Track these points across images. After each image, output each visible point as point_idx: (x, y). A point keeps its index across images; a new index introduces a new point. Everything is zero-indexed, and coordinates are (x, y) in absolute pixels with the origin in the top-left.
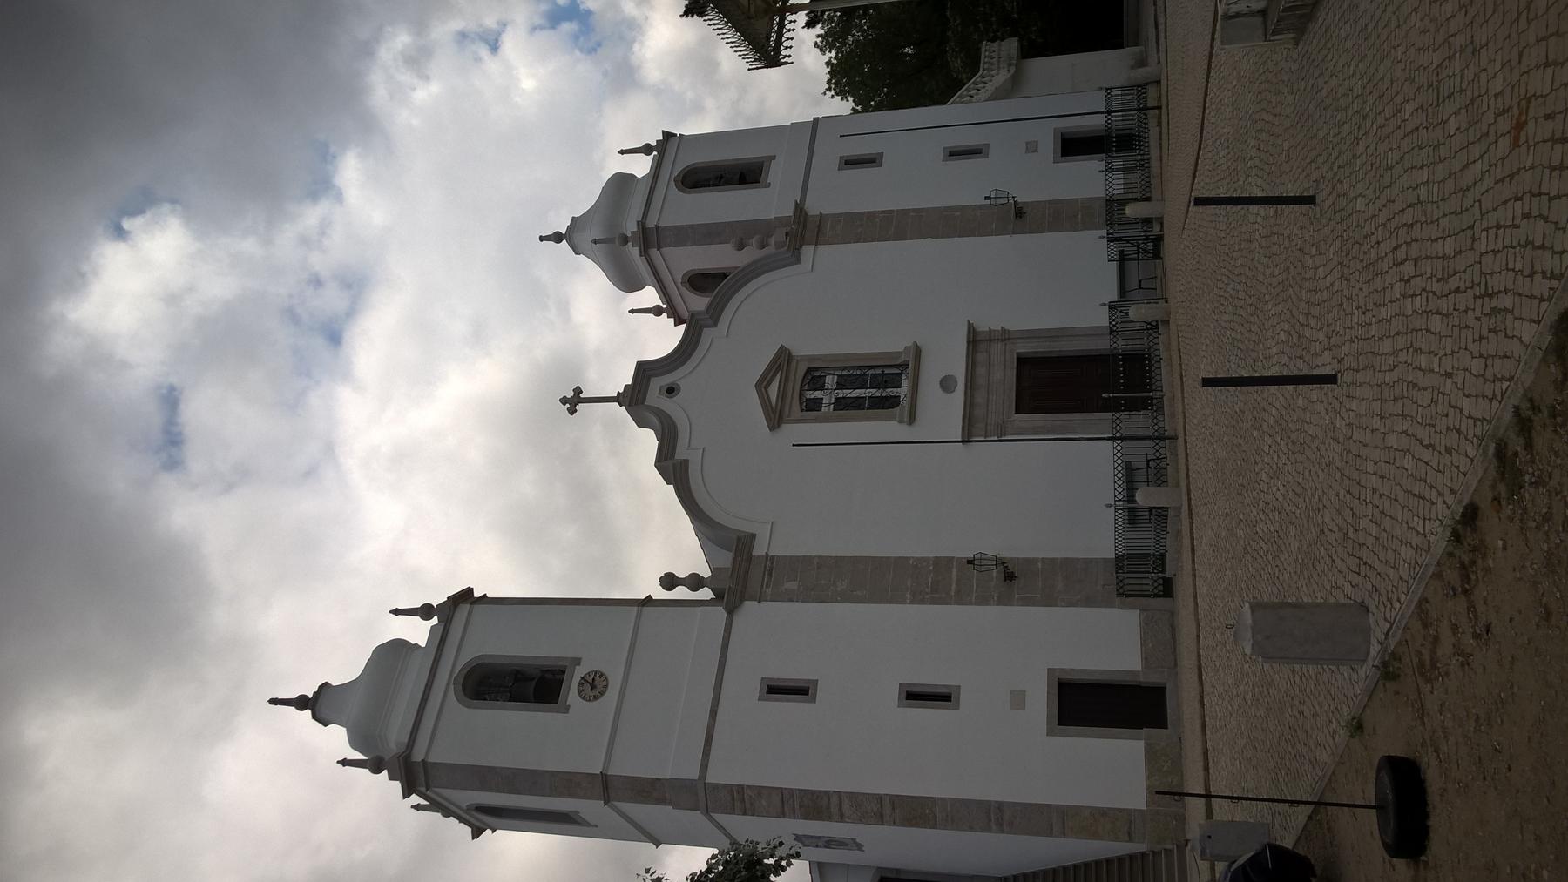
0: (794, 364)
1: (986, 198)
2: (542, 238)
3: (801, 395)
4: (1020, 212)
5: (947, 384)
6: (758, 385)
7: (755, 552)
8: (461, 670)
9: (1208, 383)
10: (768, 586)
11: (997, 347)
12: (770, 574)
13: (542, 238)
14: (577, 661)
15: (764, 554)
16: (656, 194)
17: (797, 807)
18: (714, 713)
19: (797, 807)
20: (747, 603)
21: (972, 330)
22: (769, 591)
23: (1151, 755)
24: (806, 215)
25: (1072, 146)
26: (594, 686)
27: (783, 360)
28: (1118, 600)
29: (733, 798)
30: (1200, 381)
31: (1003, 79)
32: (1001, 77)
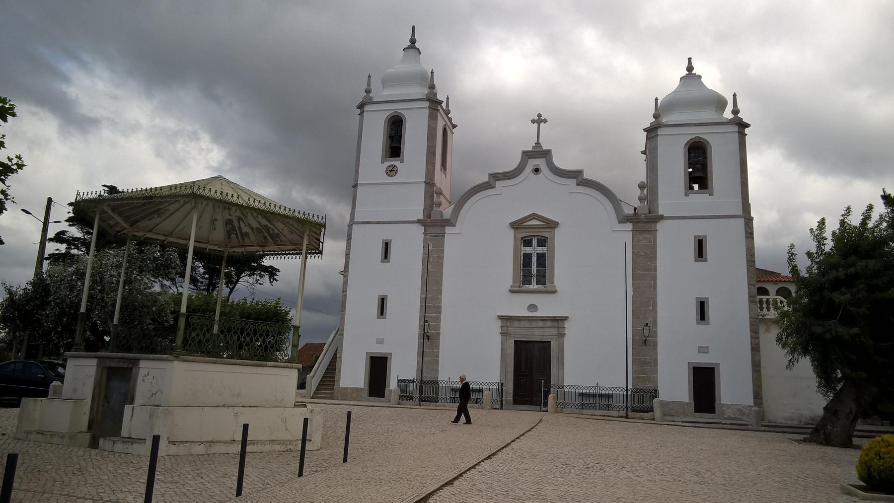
0: (549, 230)
2: (690, 59)
5: (532, 307)
6: (534, 214)
8: (400, 113)
9: (349, 413)
10: (430, 236)
12: (436, 236)
13: (690, 59)
16: (676, 129)
18: (378, 223)
21: (564, 319)
22: (429, 237)
23: (357, 390)
24: (657, 222)
26: (392, 171)
27: (552, 225)
30: (350, 411)
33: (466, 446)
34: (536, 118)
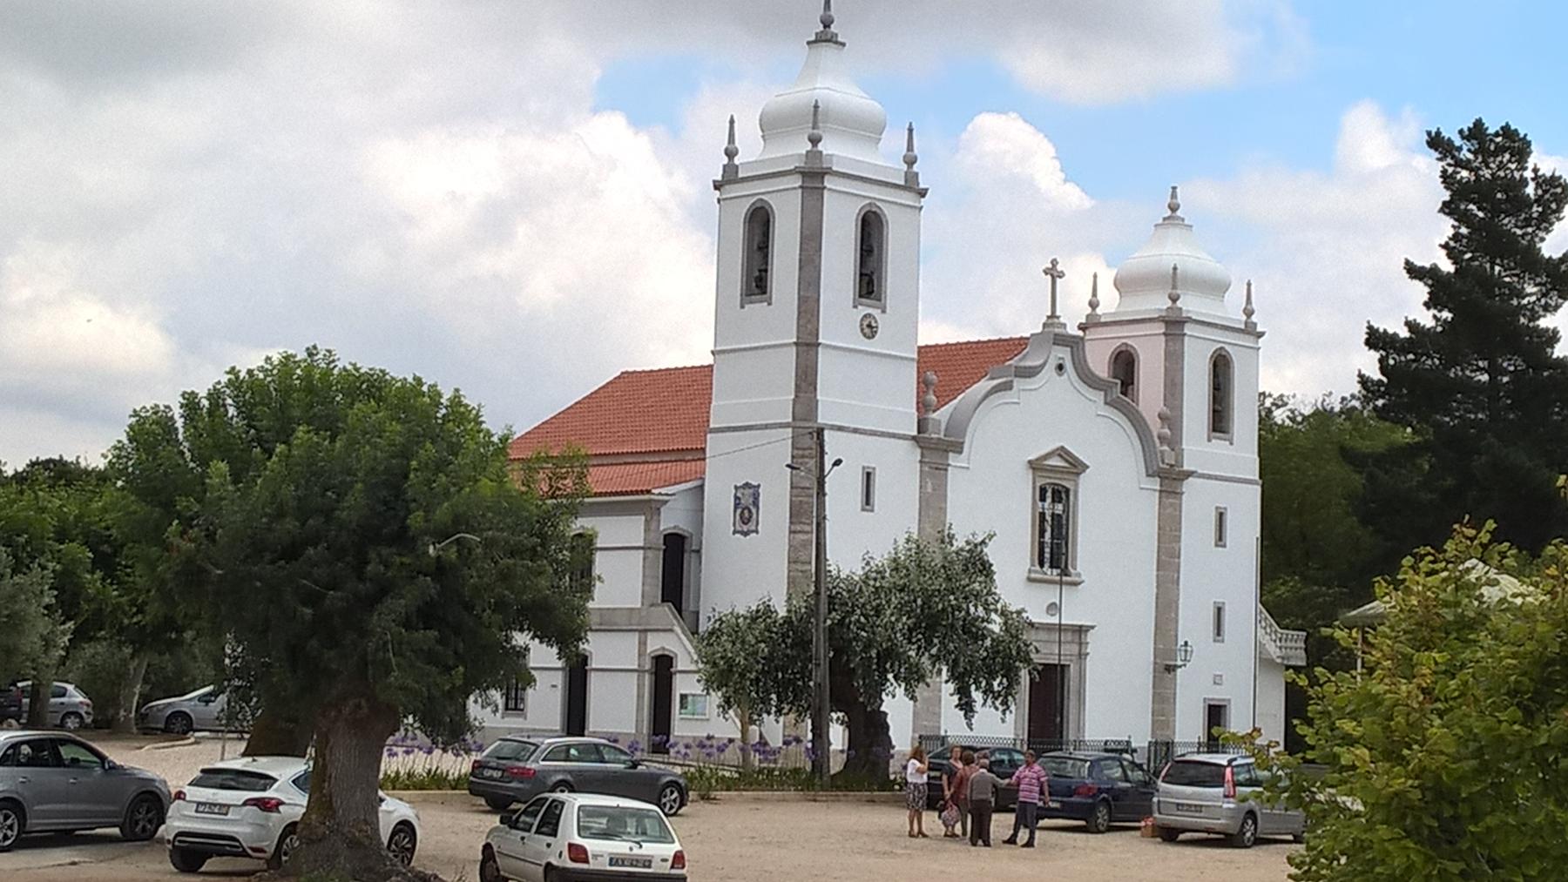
0: (1072, 477)
1: (1186, 643)
3: (1048, 484)
4: (1170, 669)
7: (951, 454)
10: (931, 468)
11: (1075, 649)
12: (937, 469)
14: (884, 312)
15: (820, 341)
16: (1209, 329)
17: (800, 499)
18: (856, 431)
19: (800, 499)
20: (918, 451)
22: (927, 469)
25: (1215, 714)
27: (1076, 467)
28: (917, 736)
29: (804, 449)
31: (1272, 653)
32: (1273, 650)
33: (962, 670)
34: (1059, 268)
